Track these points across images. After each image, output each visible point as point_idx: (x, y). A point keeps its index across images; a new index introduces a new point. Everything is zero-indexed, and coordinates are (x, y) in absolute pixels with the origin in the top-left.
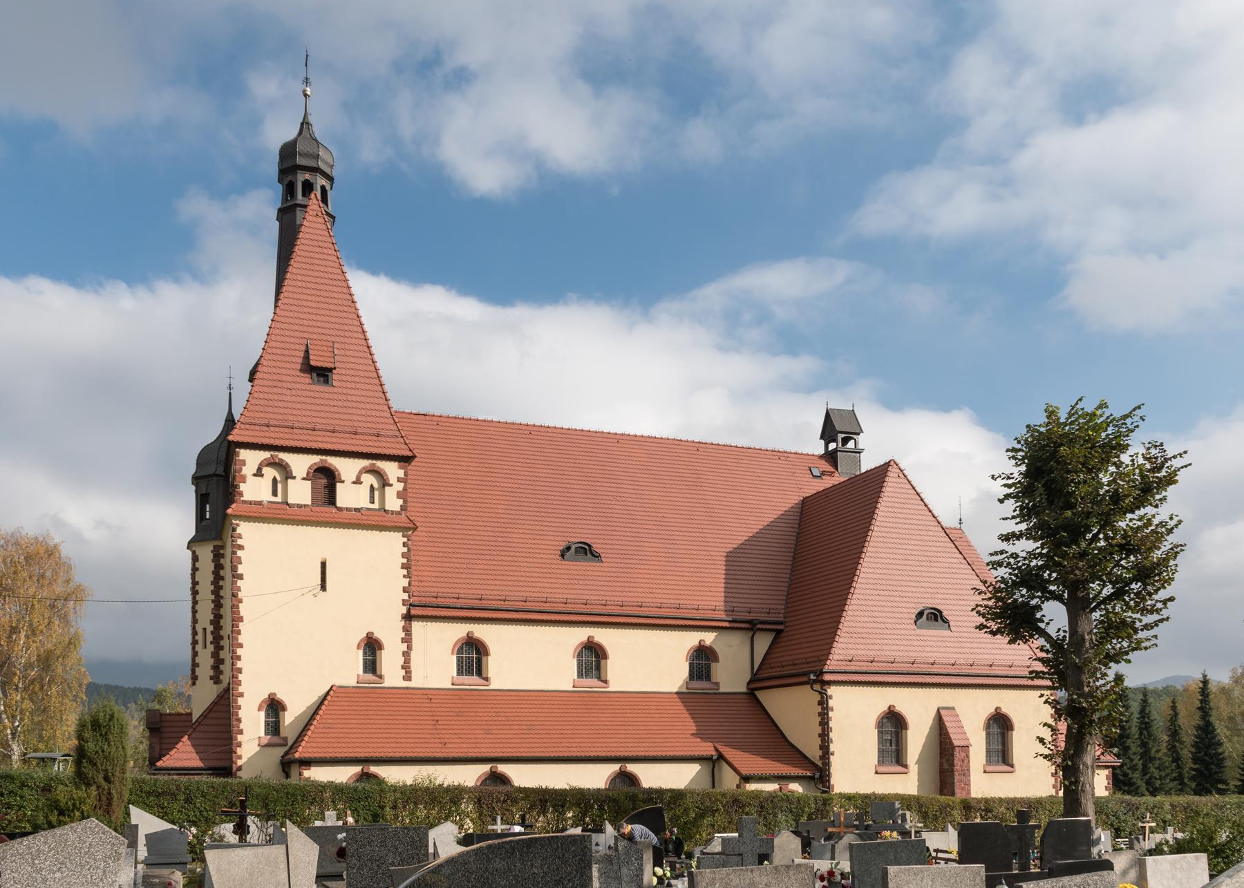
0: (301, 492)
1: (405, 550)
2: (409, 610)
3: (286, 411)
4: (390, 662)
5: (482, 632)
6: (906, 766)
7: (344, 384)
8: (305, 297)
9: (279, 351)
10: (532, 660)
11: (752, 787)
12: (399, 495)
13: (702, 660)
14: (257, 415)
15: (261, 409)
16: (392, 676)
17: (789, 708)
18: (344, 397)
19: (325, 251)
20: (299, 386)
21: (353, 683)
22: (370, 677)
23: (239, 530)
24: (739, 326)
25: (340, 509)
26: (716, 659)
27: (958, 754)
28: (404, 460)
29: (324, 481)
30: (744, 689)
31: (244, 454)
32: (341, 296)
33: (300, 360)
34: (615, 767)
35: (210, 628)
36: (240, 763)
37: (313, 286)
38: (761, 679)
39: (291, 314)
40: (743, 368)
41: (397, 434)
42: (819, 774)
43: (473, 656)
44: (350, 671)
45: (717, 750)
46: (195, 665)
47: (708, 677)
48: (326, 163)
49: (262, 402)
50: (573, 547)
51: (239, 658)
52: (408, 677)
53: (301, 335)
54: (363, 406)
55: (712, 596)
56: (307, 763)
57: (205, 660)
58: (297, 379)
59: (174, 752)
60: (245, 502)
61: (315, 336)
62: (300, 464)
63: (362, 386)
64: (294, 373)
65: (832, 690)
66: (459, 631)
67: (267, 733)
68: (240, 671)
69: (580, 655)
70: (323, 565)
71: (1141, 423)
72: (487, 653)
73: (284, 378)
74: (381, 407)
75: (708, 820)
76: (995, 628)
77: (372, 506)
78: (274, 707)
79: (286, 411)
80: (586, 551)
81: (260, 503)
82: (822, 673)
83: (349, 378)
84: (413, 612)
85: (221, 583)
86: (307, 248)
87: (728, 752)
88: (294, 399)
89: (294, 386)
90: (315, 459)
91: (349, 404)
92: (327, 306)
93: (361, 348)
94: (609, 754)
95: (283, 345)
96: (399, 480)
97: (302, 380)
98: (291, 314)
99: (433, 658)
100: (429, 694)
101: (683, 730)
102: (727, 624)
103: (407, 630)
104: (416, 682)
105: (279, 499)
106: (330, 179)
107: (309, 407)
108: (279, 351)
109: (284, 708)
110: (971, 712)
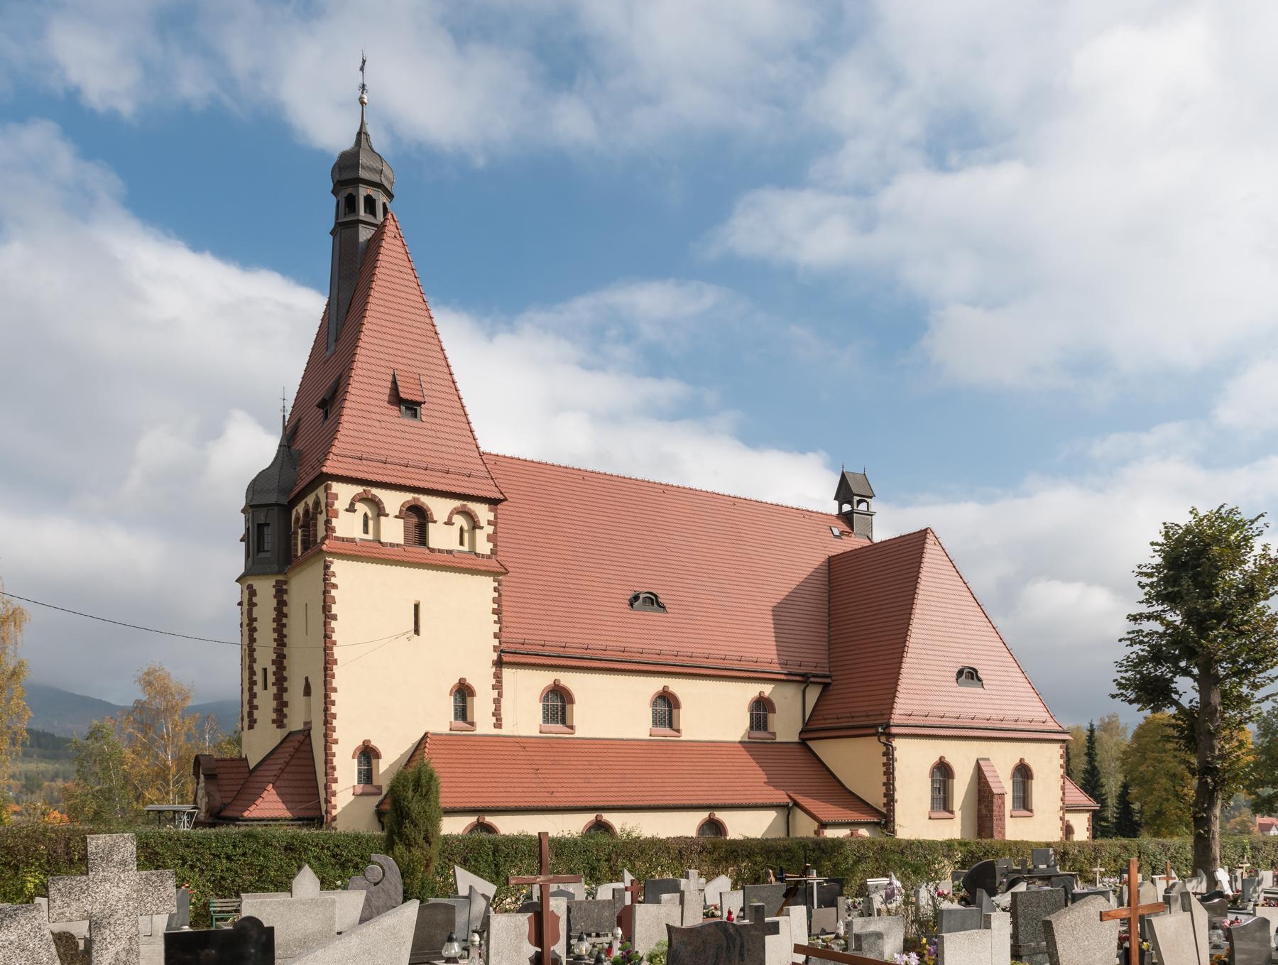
0: (393, 530)
1: (496, 595)
2: (500, 657)
3: (376, 444)
4: (481, 708)
5: (569, 680)
6: (952, 812)
7: (432, 420)
8: (389, 324)
9: (366, 380)
10: (612, 709)
11: (830, 833)
12: (490, 538)
13: (761, 709)
14: (348, 446)
15: (352, 440)
16: (483, 724)
17: (849, 759)
18: (433, 434)
19: (405, 276)
20: (388, 419)
21: (446, 730)
22: (460, 724)
23: (333, 568)
24: (601, 344)
25: (432, 550)
26: (773, 711)
27: (996, 801)
28: (493, 502)
29: (415, 520)
30: (796, 739)
31: (336, 487)
32: (424, 326)
33: (388, 391)
34: (704, 815)
35: (272, 669)
36: (334, 812)
37: (396, 313)
38: (812, 730)
39: (376, 341)
40: (607, 389)
41: (487, 475)
42: (884, 819)
43: (558, 704)
44: (441, 720)
45: (790, 797)
46: (253, 707)
47: (765, 728)
48: (388, 179)
49: (352, 433)
50: (642, 596)
51: (333, 703)
52: (498, 725)
53: (387, 364)
54: (452, 444)
55: (766, 651)
57: (266, 700)
58: (385, 411)
59: (241, 800)
60: (337, 538)
61: (400, 367)
62: (393, 501)
63: (451, 423)
64: (382, 404)
65: (896, 743)
66: (545, 679)
67: (359, 782)
68: (334, 716)
69: (654, 704)
70: (417, 607)
71: (1265, 530)
72: (572, 702)
73: (373, 409)
74: (469, 447)
75: (862, 867)
76: (1133, 697)
77: (461, 548)
78: (368, 754)
79: (376, 444)
80: (653, 601)
81: (352, 540)
82: (888, 726)
83: (437, 414)
84: (506, 658)
85: (284, 621)
86: (388, 272)
87: (801, 800)
88: (384, 432)
89: (383, 418)
90: (408, 497)
91: (439, 441)
92: (411, 336)
93: (446, 383)
94: (701, 802)
95: (370, 374)
96: (489, 523)
97: (391, 412)
98: (376, 341)
99: (521, 706)
100: (521, 743)
101: (755, 780)
102: (783, 677)
103: (498, 677)
104: (506, 730)
105: (370, 536)
106: (390, 196)
107: (399, 441)
108: (366, 380)
109: (378, 756)
110: (1001, 762)
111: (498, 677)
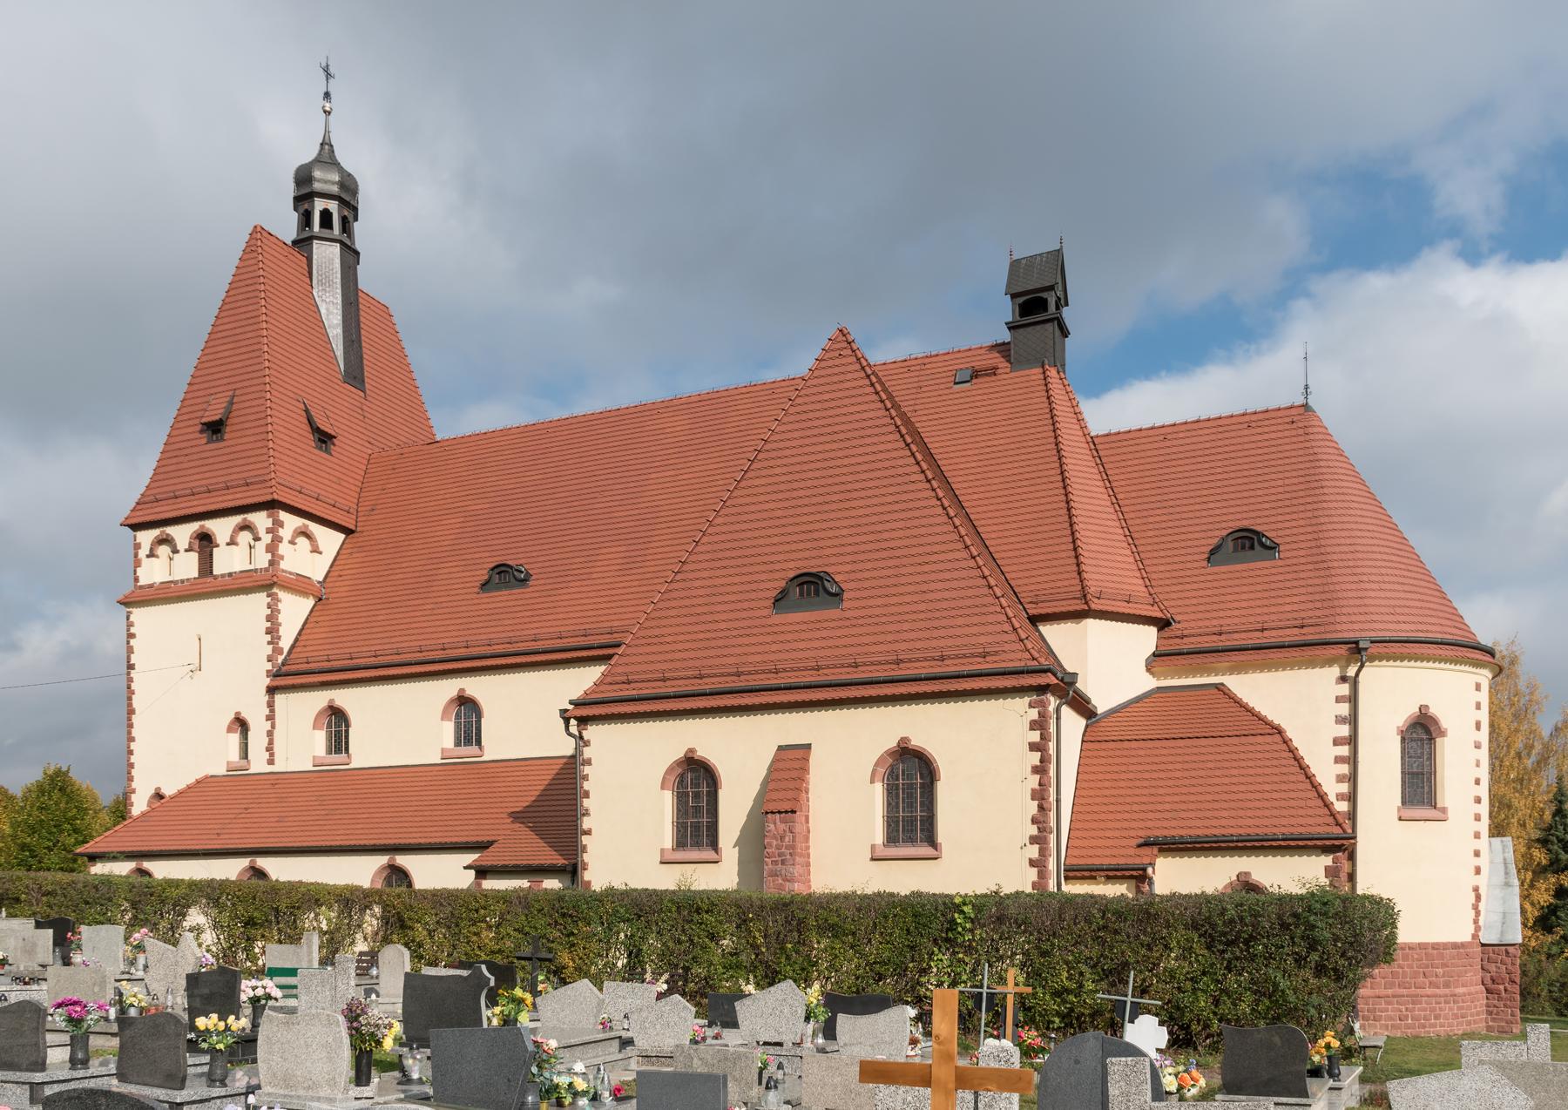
34: (383, 860)
43: (337, 722)
52: (271, 762)
56: (93, 858)
62: (183, 534)
103: (271, 705)
104: (279, 767)
111: (271, 705)
